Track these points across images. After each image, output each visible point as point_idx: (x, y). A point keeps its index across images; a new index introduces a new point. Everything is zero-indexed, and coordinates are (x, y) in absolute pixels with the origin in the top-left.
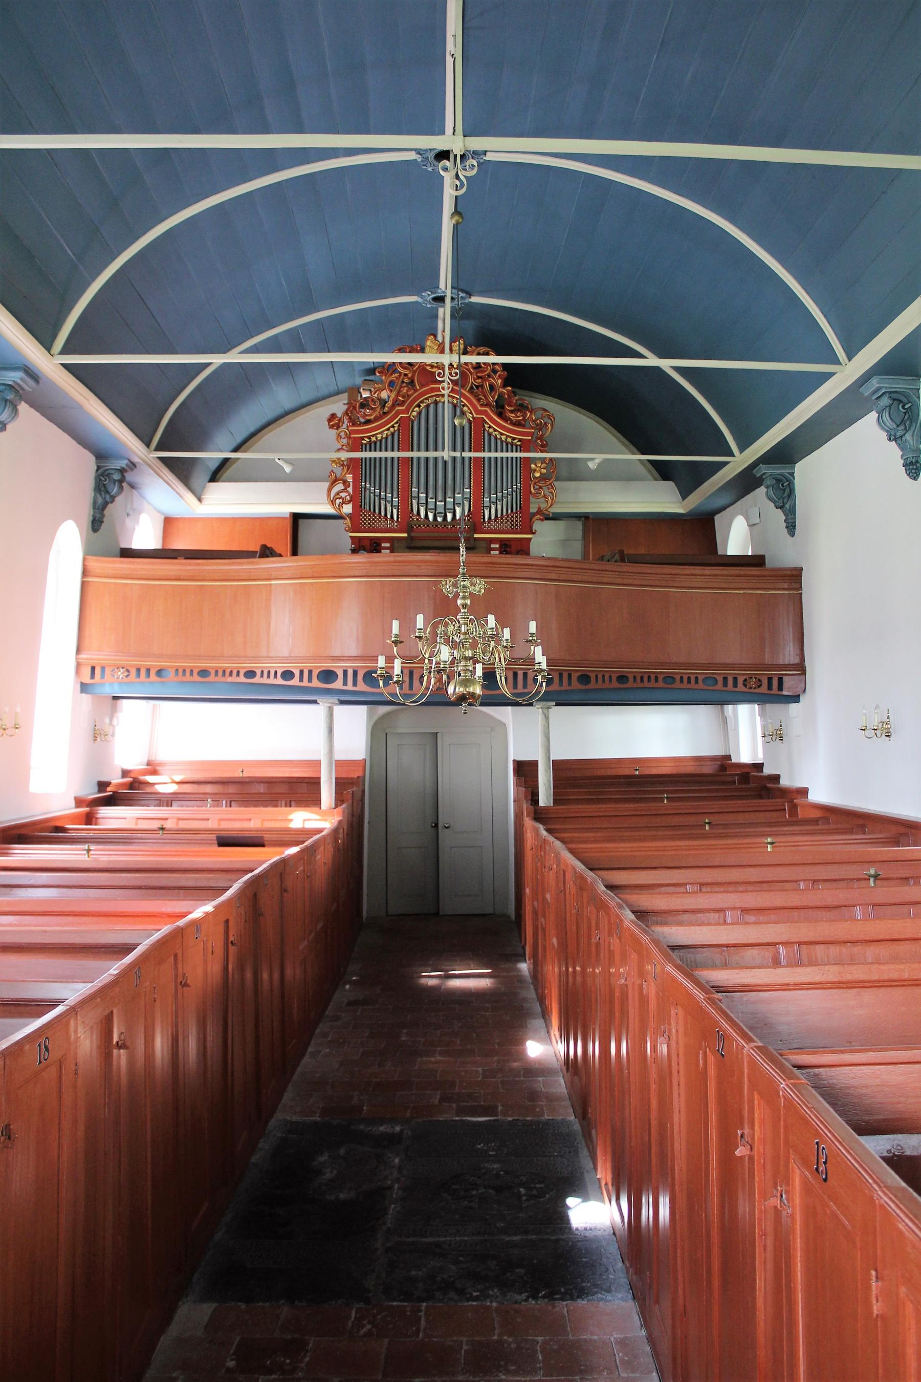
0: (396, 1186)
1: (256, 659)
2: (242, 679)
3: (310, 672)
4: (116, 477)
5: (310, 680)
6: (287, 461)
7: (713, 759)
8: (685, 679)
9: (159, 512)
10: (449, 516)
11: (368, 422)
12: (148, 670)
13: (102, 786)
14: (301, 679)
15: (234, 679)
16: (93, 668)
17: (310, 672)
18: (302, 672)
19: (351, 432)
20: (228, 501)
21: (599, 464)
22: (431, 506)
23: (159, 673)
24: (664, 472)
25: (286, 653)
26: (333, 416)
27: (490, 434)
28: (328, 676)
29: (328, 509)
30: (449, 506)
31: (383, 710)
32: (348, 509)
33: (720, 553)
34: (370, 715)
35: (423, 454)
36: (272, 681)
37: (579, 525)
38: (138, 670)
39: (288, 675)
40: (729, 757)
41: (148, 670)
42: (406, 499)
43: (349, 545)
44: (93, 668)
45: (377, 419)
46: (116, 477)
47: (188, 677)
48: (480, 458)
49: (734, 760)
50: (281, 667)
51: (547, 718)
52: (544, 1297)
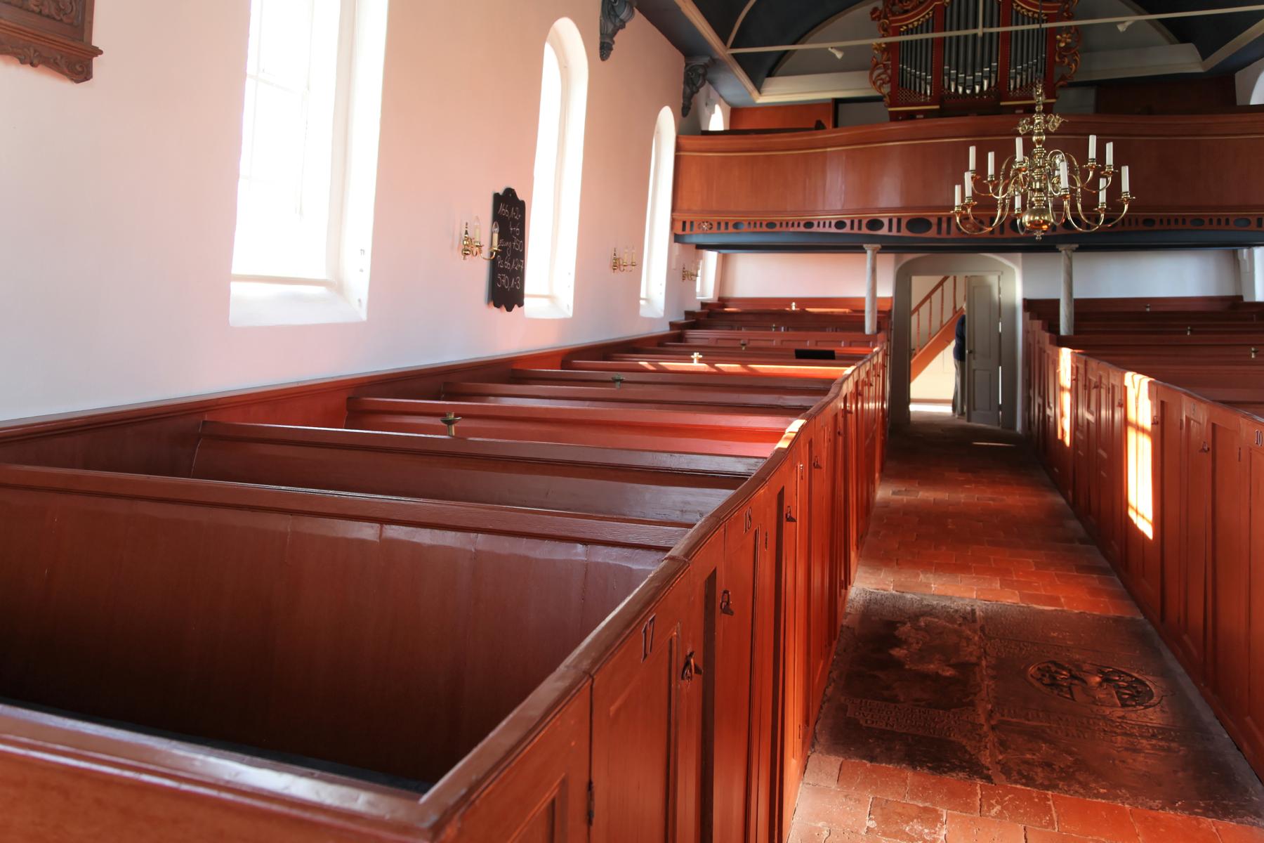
0: (984, 663)
1: (814, 213)
2: (802, 229)
3: (860, 222)
4: (701, 71)
5: (860, 228)
6: (839, 49)
7: (1222, 299)
8: (1223, 221)
9: (728, 103)
10: (977, 88)
11: (907, 12)
12: (727, 224)
13: (688, 314)
14: (852, 228)
15: (795, 229)
16: (684, 223)
17: (860, 222)
18: (852, 222)
19: (891, 22)
20: (781, 92)
21: (1129, 28)
22: (961, 81)
23: (736, 225)
24: (1180, 32)
25: (839, 207)
26: (875, 10)
27: (1017, 12)
28: (875, 224)
29: (873, 93)
30: (977, 80)
31: (908, 257)
32: (886, 89)
33: (1240, 102)
34: (897, 261)
35: (955, 33)
36: (827, 230)
37: (1091, 95)
38: (719, 224)
39: (840, 224)
40: (1241, 298)
41: (727, 224)
42: (938, 75)
43: (888, 118)
44: (684, 223)
45: (913, 9)
46: (701, 71)
47: (758, 229)
48: (1004, 25)
49: (1246, 299)
50: (834, 218)
51: (1070, 259)
52: (1183, 809)
